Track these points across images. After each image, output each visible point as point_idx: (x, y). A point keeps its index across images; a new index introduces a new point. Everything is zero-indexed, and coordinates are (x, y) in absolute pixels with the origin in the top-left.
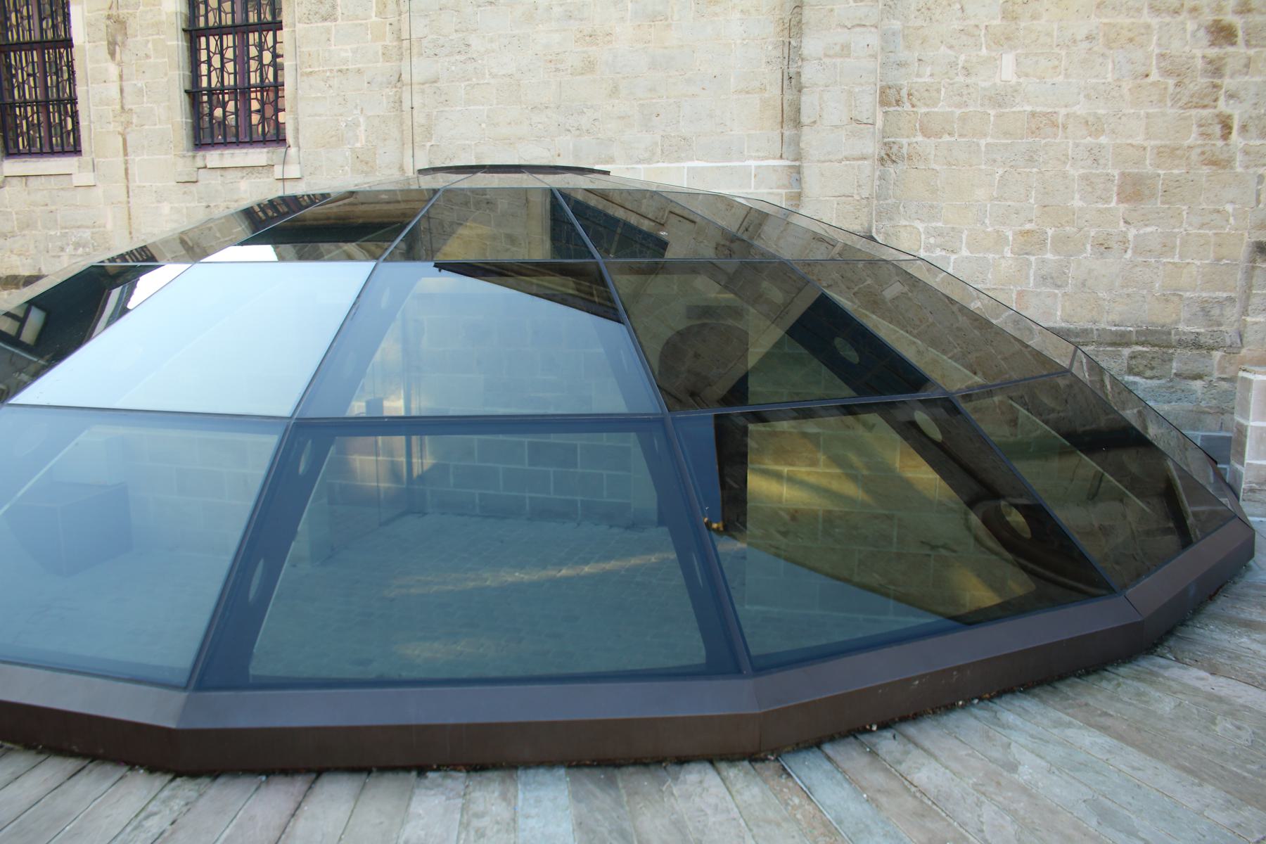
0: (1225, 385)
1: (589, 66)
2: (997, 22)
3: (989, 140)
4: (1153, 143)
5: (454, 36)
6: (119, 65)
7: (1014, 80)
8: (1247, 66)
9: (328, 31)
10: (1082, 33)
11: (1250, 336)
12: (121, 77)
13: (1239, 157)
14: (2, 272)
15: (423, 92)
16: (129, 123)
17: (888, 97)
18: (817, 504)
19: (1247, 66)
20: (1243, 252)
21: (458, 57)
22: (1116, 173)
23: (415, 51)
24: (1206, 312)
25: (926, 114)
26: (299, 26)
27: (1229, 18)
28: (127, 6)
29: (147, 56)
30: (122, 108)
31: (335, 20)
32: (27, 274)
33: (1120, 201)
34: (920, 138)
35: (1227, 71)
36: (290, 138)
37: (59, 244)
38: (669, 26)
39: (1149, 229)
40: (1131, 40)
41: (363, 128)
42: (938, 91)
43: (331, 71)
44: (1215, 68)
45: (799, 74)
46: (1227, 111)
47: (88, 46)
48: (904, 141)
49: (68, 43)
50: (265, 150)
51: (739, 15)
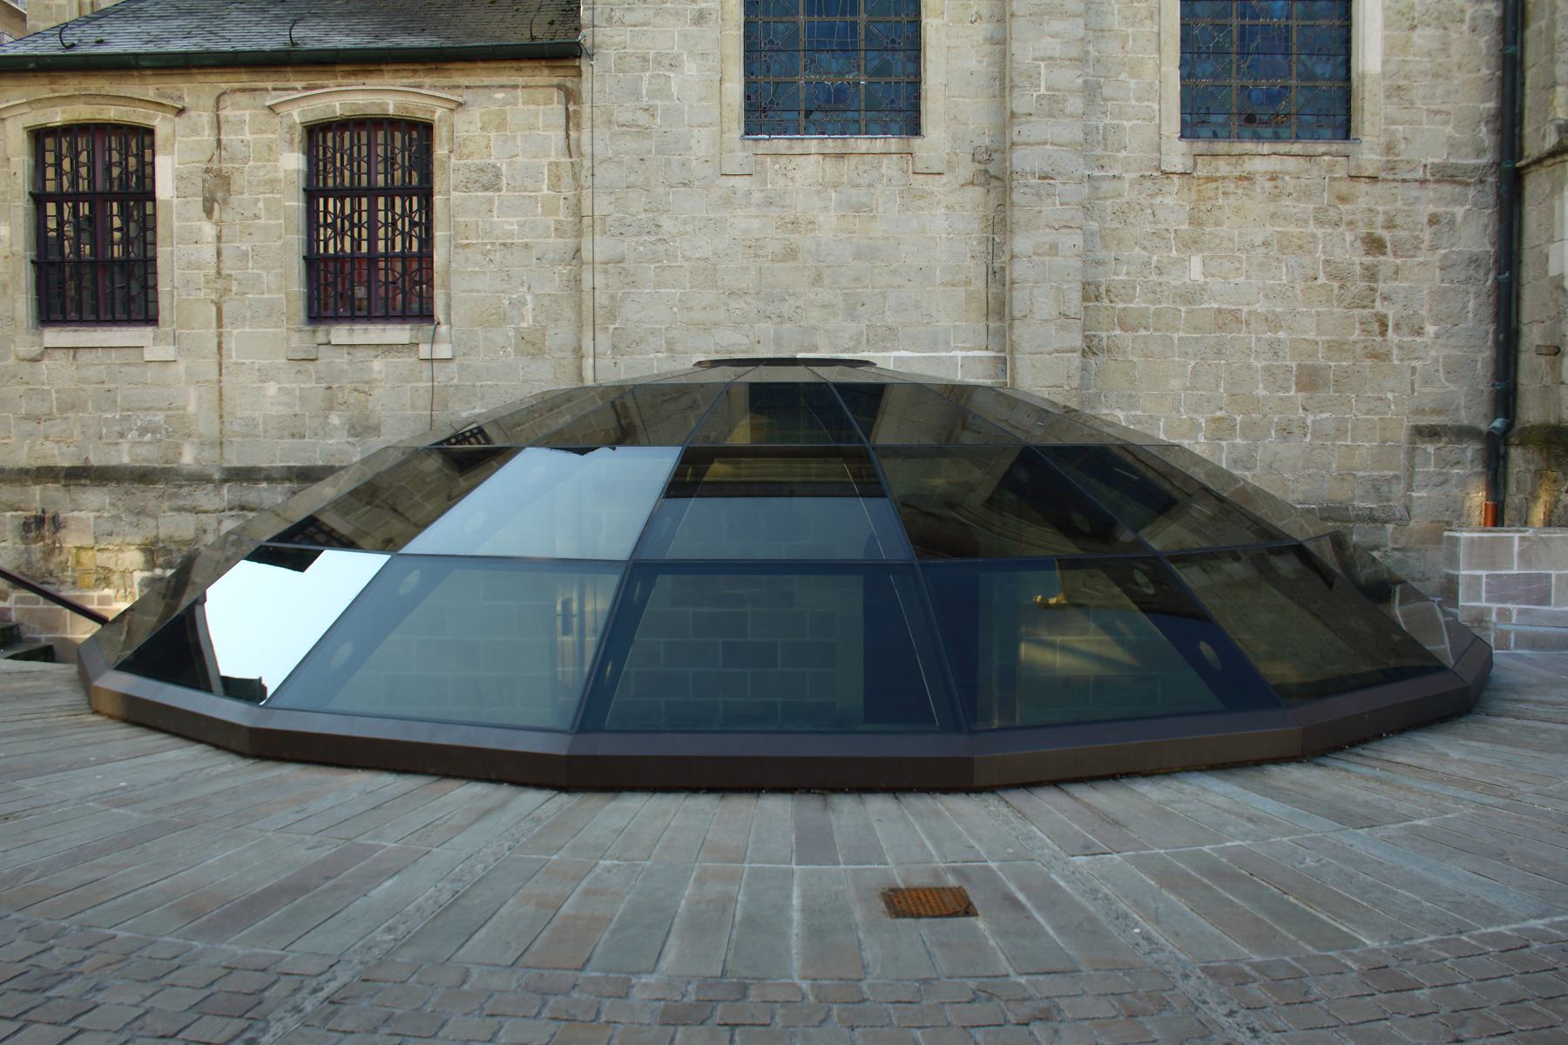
0: (1398, 555)
1: (791, 253)
3: (1181, 334)
5: (643, 216)
7: (1202, 280)
8: (1396, 273)
9: (490, 201)
11: (1415, 511)
12: (219, 238)
13: (1395, 351)
15: (606, 272)
16: (227, 290)
17: (1090, 292)
18: (1090, 669)
19: (1396, 273)
20: (1403, 435)
23: (597, 229)
24: (1377, 489)
26: (454, 194)
27: (1380, 232)
28: (232, 160)
29: (256, 217)
30: (219, 273)
31: (499, 190)
32: (67, 464)
33: (1298, 390)
34: (1118, 332)
35: (1381, 276)
36: (439, 313)
37: (118, 428)
38: (874, 217)
39: (1324, 415)
40: (1301, 247)
41: (530, 306)
42: (1134, 288)
43: (493, 244)
44: (1371, 274)
45: (1003, 269)
46: (1384, 311)
47: (175, 201)
48: (1104, 334)
49: (151, 196)
50: (408, 326)
51: (944, 211)
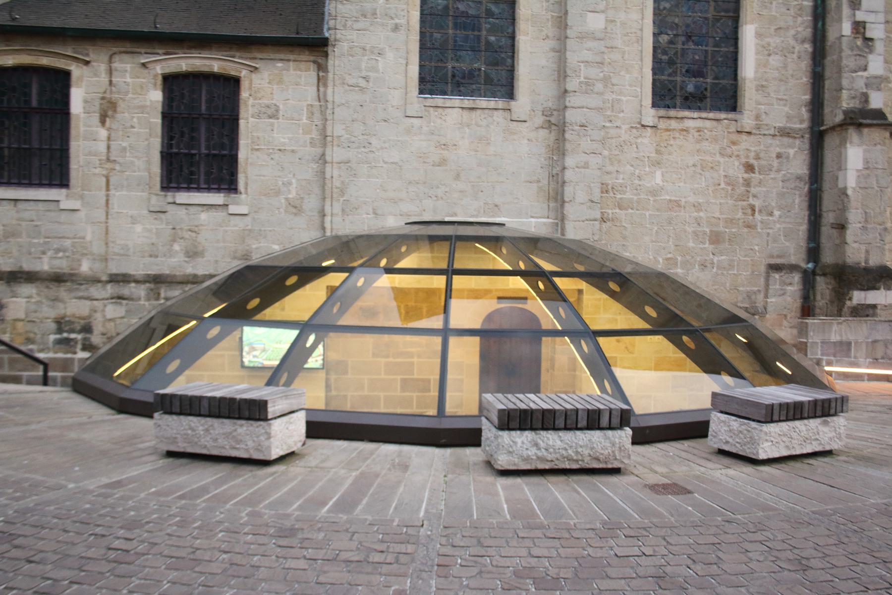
1: (443, 162)
2: (653, 155)
3: (651, 212)
4: (723, 216)
5: (361, 137)
6: (109, 129)
9: (272, 125)
10: (691, 164)
11: (769, 309)
13: (759, 224)
14: (6, 265)
15: (340, 168)
20: (763, 269)
21: (363, 149)
22: (708, 230)
25: (621, 199)
27: (752, 161)
29: (133, 127)
31: (278, 119)
33: (710, 244)
34: (617, 211)
35: (752, 184)
37: (42, 249)
39: (723, 258)
41: (294, 186)
48: (610, 211)
51: (526, 141)
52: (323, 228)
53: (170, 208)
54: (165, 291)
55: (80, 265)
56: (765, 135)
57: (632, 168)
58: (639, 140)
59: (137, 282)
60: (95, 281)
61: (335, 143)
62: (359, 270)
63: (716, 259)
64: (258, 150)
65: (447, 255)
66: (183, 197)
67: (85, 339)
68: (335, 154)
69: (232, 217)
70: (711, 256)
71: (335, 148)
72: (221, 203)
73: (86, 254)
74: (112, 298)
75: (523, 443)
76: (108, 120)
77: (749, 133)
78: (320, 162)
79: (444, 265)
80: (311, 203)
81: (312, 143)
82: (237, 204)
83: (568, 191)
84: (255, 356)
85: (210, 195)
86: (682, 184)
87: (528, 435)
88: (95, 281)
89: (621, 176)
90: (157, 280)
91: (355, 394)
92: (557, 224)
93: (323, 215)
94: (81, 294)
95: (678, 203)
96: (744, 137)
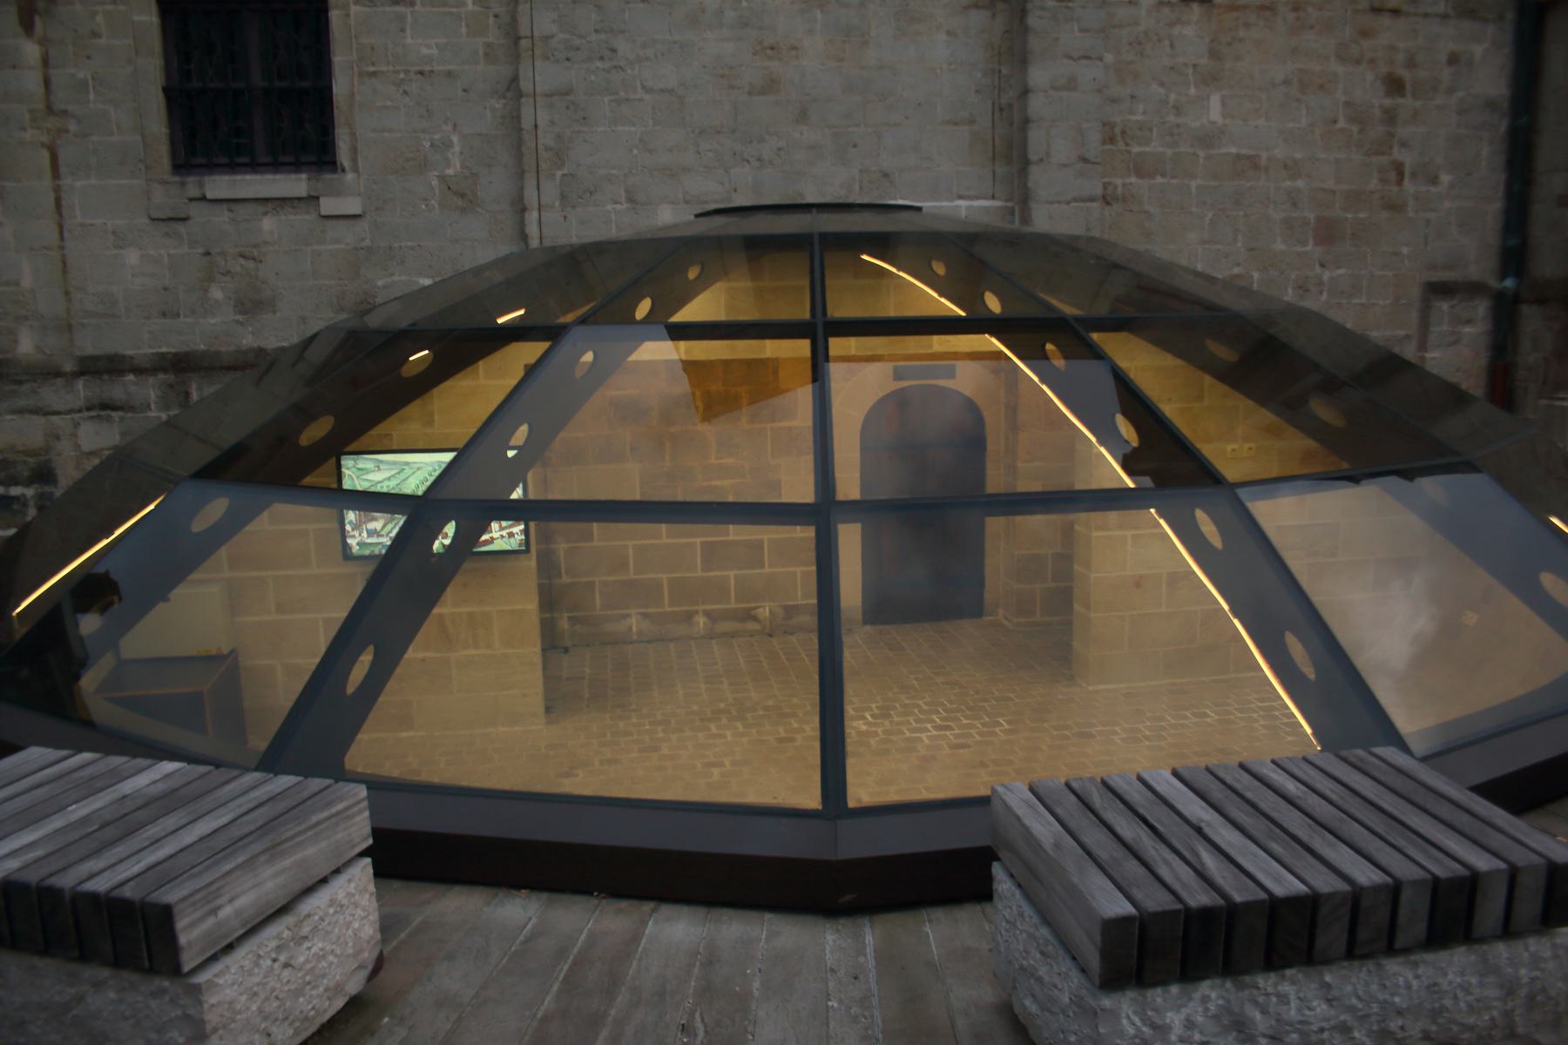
1: (770, 85)
2: (1204, 61)
3: (1199, 182)
5: (594, 37)
6: (43, 42)
12: (45, 62)
20: (1415, 292)
21: (599, 64)
22: (1311, 216)
25: (1140, 154)
27: (1402, 72)
29: (95, 35)
34: (1133, 180)
39: (1341, 271)
41: (457, 149)
48: (1119, 182)
51: (944, 37)
52: (524, 237)
53: (194, 210)
54: (200, 389)
55: (16, 341)
56: (1426, 15)
57: (1161, 90)
58: (1176, 31)
59: (139, 371)
60: (49, 373)
61: (538, 52)
62: (578, 333)
63: (1326, 275)
64: (374, 74)
65: (806, 282)
66: (220, 185)
67: (41, 497)
68: (542, 76)
69: (329, 223)
70: (1318, 269)
71: (538, 64)
72: (304, 194)
73: (26, 318)
74: (89, 409)
75: (1190, 1024)
76: (38, 21)
77: (1396, 12)
78: (509, 94)
79: (801, 311)
80: (495, 185)
81: (489, 55)
82: (338, 193)
83: (1036, 137)
84: (371, 533)
85: (278, 177)
86: (1261, 122)
87: (1211, 993)
88: (49, 373)
89: (1141, 107)
90: (181, 365)
91: (611, 578)
92: (1012, 212)
93: (521, 209)
94: (22, 403)
95: (1253, 162)
96: (1386, 20)
